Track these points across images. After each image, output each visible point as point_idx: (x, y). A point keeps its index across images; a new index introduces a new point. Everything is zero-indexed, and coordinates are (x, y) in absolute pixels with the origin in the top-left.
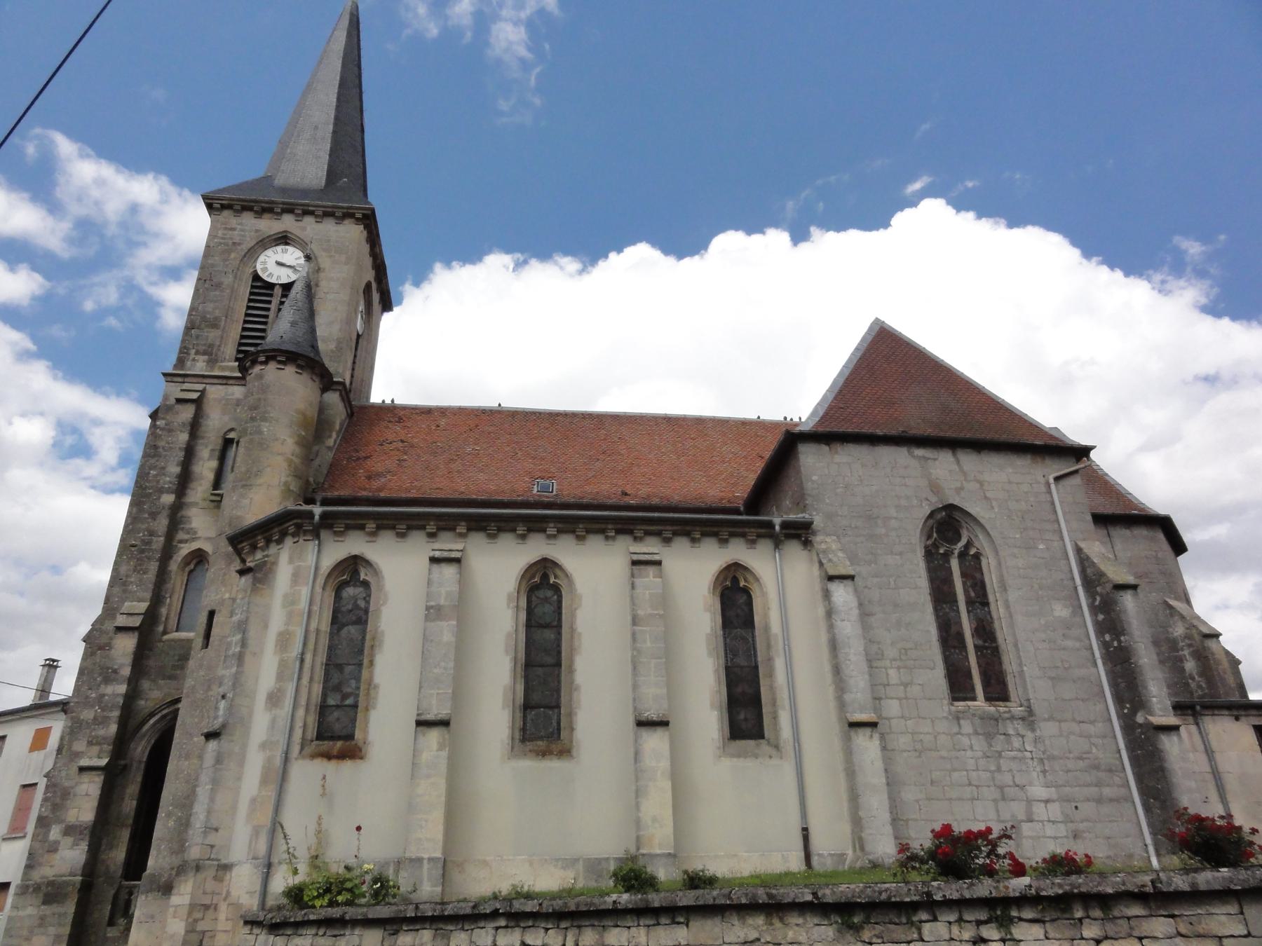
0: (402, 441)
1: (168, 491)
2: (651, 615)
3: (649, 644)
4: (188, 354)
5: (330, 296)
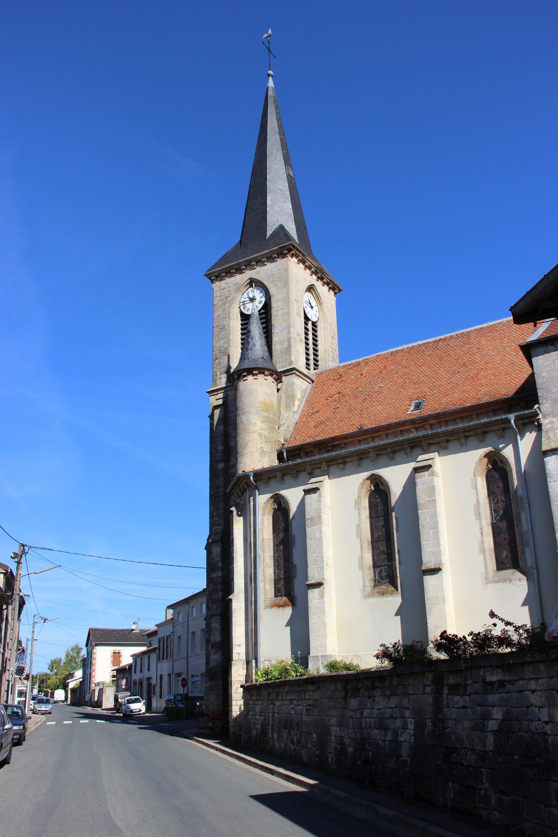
0: (339, 393)
1: (221, 461)
2: (428, 501)
3: (428, 520)
4: (217, 375)
5: (279, 313)
